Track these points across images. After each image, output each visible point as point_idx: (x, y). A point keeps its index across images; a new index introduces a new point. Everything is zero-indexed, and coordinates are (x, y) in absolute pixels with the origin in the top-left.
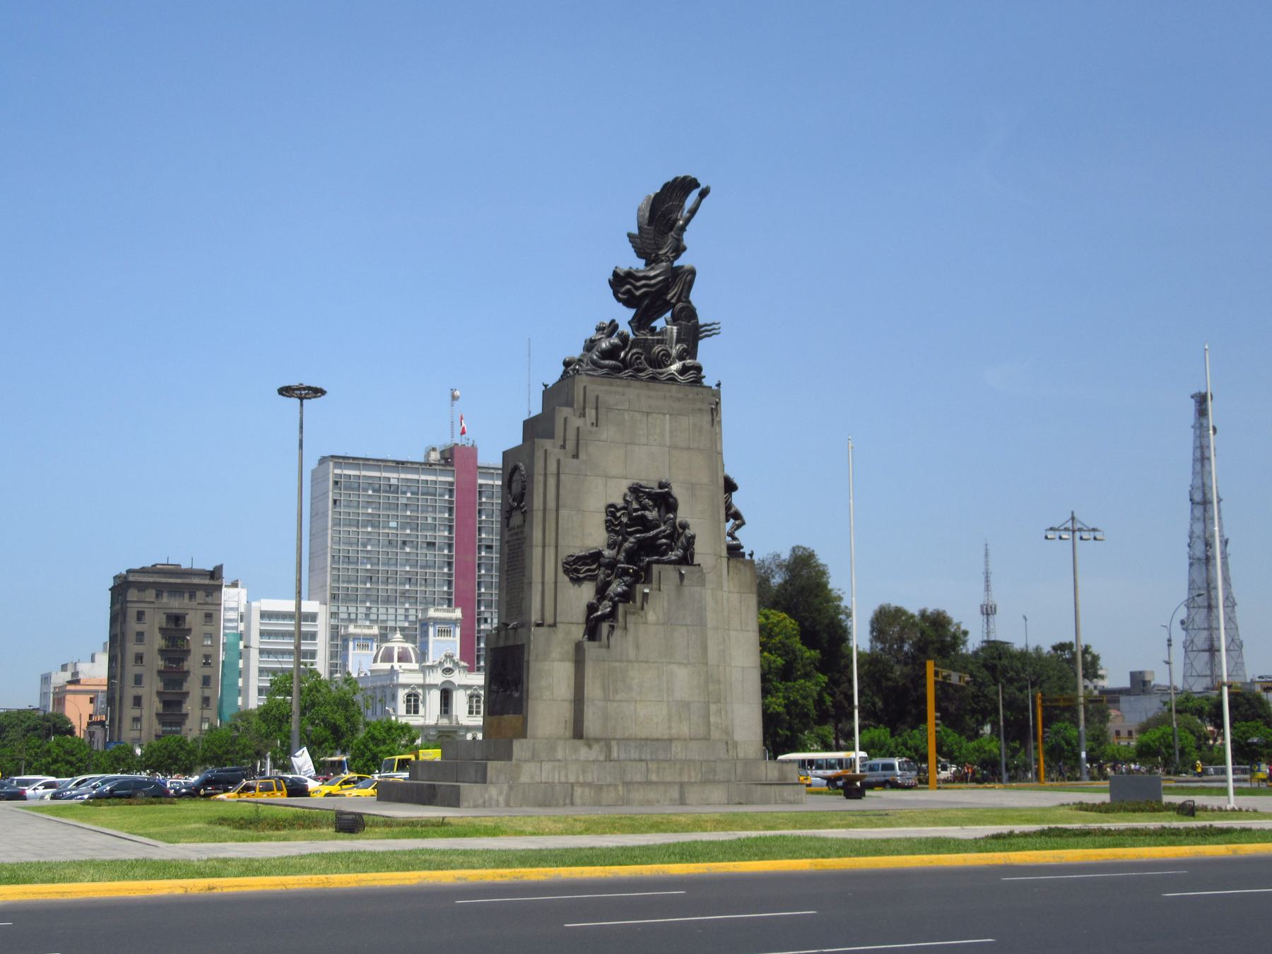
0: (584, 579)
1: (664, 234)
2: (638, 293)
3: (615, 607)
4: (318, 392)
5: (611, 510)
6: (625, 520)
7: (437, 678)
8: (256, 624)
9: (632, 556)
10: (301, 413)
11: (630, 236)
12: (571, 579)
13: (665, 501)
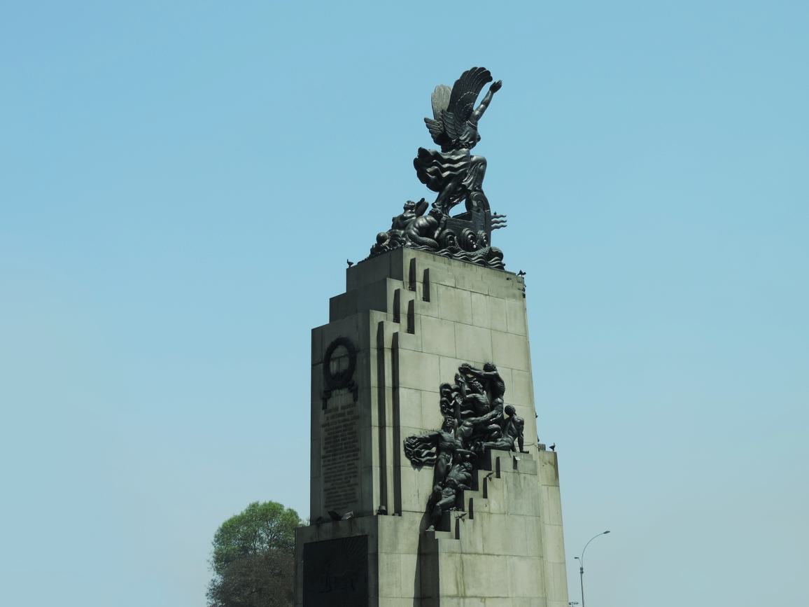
1: (462, 121)
5: (445, 391)
6: (460, 402)
13: (493, 383)
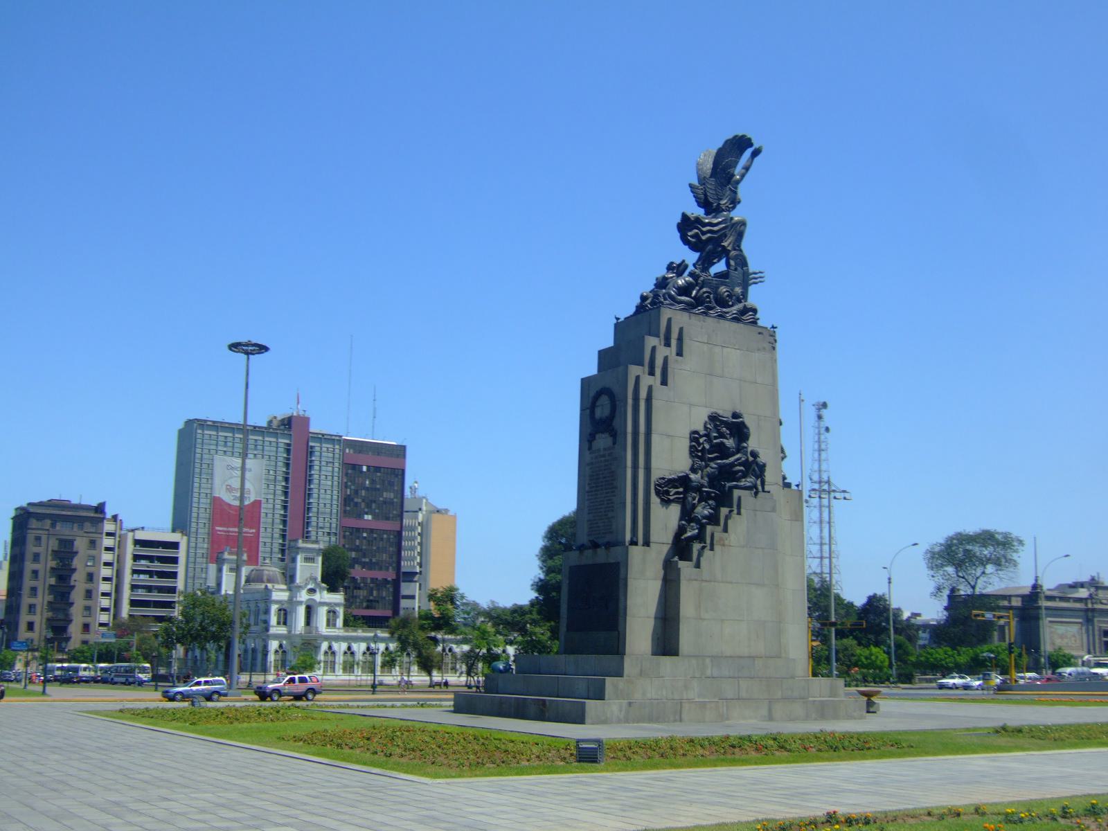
0: (673, 501)
2: (704, 238)
3: (702, 528)
4: (262, 349)
5: (694, 437)
7: (303, 596)
8: (130, 549)
9: (713, 480)
10: (248, 366)
11: (691, 186)
12: (662, 500)
13: (739, 430)
